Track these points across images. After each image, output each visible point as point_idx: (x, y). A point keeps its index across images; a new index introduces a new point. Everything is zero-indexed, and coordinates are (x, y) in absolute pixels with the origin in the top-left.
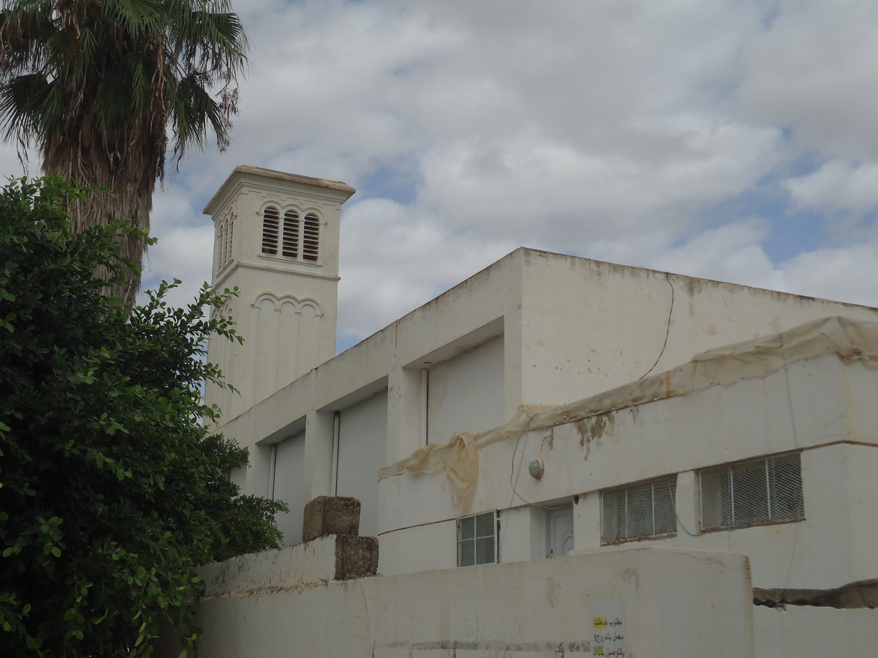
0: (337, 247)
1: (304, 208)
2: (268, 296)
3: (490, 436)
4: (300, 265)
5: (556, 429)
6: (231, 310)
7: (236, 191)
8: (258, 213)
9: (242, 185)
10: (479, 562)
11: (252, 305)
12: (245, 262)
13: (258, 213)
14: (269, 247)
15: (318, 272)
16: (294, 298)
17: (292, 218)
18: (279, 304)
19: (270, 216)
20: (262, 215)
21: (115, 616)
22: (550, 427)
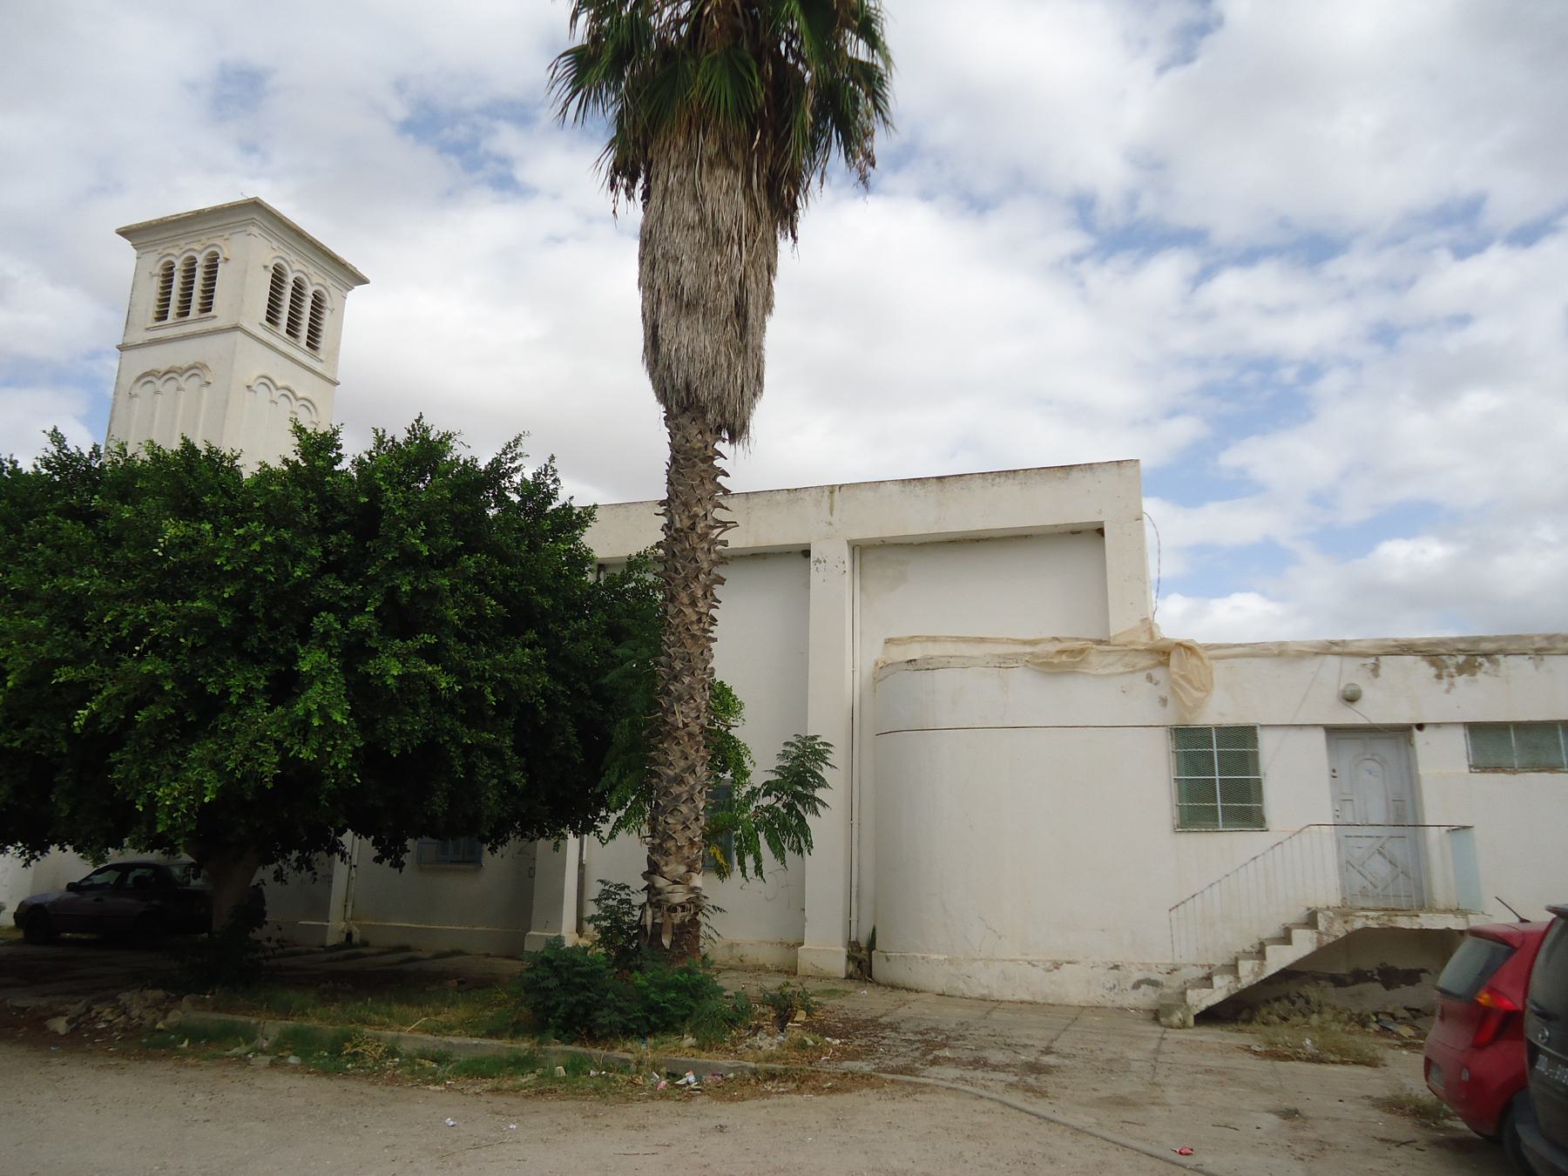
0: (339, 343)
1: (314, 281)
2: (267, 382)
3: (1247, 650)
4: (300, 352)
5: (1382, 659)
6: (209, 383)
7: (231, 225)
8: (265, 267)
9: (254, 223)
10: (1256, 747)
11: (248, 387)
12: (246, 325)
13: (265, 267)
14: (272, 315)
15: (318, 367)
16: (293, 393)
17: (298, 288)
18: (276, 394)
19: (278, 278)
20: (270, 271)
21: (1457, 663)
22: (1377, 656)
